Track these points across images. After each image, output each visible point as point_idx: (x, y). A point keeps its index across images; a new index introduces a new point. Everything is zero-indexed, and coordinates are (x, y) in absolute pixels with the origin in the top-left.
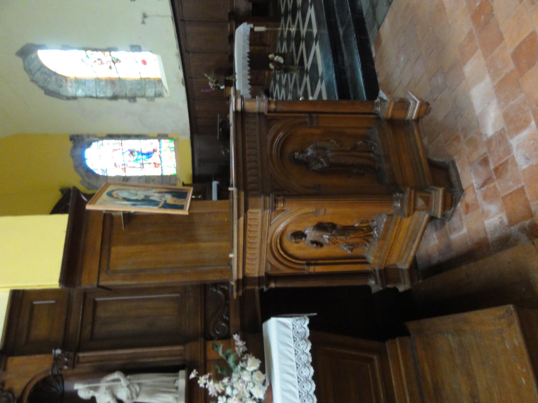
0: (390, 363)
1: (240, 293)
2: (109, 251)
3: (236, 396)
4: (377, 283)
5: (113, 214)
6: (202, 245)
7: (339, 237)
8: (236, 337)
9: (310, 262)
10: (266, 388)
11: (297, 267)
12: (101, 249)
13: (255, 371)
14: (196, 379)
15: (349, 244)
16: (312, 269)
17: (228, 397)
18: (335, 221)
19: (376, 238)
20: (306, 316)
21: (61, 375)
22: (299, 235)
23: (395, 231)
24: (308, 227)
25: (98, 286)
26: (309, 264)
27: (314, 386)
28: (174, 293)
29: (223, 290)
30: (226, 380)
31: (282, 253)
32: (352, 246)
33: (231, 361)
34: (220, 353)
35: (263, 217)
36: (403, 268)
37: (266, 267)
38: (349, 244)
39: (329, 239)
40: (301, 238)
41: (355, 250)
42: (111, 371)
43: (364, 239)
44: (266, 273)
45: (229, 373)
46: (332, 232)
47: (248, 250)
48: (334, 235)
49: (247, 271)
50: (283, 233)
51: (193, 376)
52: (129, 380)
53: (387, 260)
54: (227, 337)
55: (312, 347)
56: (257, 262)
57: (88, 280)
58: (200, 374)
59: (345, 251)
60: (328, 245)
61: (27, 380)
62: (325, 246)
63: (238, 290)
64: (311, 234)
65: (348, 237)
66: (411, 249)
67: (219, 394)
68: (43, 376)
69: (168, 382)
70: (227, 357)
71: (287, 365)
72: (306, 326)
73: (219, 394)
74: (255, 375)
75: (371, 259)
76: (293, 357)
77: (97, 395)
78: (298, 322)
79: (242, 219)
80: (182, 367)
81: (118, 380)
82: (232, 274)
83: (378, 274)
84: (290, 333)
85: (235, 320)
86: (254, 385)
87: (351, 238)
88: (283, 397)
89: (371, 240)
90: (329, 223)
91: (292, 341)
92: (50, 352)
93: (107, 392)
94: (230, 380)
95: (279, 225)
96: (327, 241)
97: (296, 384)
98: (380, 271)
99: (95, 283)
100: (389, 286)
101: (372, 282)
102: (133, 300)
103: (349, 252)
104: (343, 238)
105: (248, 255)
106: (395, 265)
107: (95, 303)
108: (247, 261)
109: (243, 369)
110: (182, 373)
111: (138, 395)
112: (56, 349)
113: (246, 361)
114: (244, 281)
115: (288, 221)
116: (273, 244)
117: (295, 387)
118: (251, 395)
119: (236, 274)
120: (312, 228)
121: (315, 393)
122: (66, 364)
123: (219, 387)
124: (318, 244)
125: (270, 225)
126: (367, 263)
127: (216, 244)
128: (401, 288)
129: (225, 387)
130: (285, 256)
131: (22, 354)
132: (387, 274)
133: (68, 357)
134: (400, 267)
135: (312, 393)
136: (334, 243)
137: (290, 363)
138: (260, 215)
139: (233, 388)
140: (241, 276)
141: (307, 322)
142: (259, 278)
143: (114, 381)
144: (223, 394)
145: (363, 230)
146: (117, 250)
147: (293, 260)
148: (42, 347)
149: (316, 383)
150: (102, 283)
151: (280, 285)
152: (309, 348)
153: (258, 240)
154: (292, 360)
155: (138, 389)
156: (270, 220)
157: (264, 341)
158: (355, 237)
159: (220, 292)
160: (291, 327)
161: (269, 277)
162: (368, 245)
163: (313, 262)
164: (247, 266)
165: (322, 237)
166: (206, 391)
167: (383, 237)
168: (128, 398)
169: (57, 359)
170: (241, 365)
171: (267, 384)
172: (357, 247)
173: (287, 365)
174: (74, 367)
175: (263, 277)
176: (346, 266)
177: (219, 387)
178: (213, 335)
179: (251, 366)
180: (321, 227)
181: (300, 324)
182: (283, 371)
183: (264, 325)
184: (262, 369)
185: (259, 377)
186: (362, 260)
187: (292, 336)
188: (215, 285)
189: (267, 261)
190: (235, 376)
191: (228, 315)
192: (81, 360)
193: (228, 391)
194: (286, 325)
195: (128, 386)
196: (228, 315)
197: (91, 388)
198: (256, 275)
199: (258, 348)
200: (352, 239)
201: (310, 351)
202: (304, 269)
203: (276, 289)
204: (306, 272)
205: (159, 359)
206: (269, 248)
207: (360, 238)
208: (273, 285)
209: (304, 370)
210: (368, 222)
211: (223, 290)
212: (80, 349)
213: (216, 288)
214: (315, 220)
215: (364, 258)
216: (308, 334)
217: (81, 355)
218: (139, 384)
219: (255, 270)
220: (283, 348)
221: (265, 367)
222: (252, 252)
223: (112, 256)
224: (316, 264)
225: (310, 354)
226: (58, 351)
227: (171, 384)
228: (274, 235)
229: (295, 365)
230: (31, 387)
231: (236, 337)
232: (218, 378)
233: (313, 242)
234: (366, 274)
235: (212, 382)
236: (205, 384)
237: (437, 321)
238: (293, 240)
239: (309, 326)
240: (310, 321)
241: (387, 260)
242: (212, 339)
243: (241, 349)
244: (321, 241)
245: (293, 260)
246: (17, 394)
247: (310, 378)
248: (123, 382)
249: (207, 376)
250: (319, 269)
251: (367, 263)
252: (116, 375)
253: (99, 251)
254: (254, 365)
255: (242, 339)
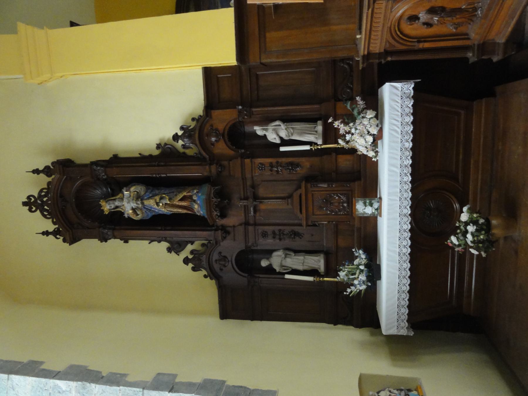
0: (474, 117)
1: (365, 65)
2: (265, 36)
3: (358, 133)
4: (473, 55)
5: (264, 5)
6: (334, 28)
7: (446, 19)
8: (358, 98)
9: (420, 39)
10: (378, 128)
11: (409, 44)
12: (259, 34)
13: (372, 118)
14: (332, 123)
15: (455, 24)
16: (421, 46)
17: (353, 134)
18: (445, 5)
19: (479, 17)
20: (412, 81)
21: (243, 122)
22: (414, 18)
23: (497, 10)
24: (422, 11)
25: (261, 63)
26: (419, 42)
27: (412, 127)
28: (312, 68)
29: (348, 64)
30: (351, 124)
31: (398, 33)
32: (457, 25)
33: (355, 112)
34: (348, 107)
35: (386, 7)
36: (500, 42)
37: (386, 44)
38: (455, 24)
39: (438, 20)
40: (415, 21)
41: (459, 28)
42: (275, 120)
43: (469, 19)
44: (384, 50)
45: (354, 120)
46: (441, 14)
47: (373, 33)
48: (442, 17)
49: (371, 48)
50: (401, 17)
51: (330, 121)
52: (286, 125)
53: (486, 36)
54: (352, 99)
55: (414, 103)
56: (378, 42)
57: (254, 59)
58: (335, 120)
59: (452, 29)
60: (437, 25)
61: (225, 124)
62: (434, 26)
63: (363, 63)
64: (423, 17)
65: (454, 18)
66: (509, 26)
67: (347, 133)
68: (233, 122)
69: (311, 128)
70: (353, 109)
71: (394, 114)
72: (411, 88)
73: (347, 133)
74: (372, 120)
75: (473, 35)
76: (400, 110)
77: (267, 134)
78: (406, 86)
79: (370, 10)
80: (320, 119)
81: (280, 125)
82: (357, 52)
83: (476, 48)
84: (399, 93)
85: (357, 87)
86: (371, 126)
87: (457, 19)
88: (390, 133)
89: (475, 19)
90: (439, 7)
91: (400, 98)
92: (235, 108)
93: (273, 132)
94: (354, 124)
95: (398, 11)
96: (436, 22)
97: (400, 126)
98: (479, 45)
99: (259, 61)
100: (483, 57)
101: (470, 55)
102: (296, 72)
103: (454, 30)
104: (449, 19)
105: (372, 37)
106: (493, 40)
107: (257, 75)
108: (372, 41)
109: (363, 117)
110: (319, 122)
111: (292, 135)
112: (238, 106)
113: (366, 113)
114: (368, 57)
115: (405, 8)
116: (392, 26)
117: (398, 128)
118: (369, 132)
119: (362, 50)
120: (424, 12)
121: (412, 132)
122: (246, 115)
123: (347, 129)
124: (428, 25)
125: (391, 12)
126: (469, 39)
127: (344, 27)
128: (495, 59)
129: (351, 128)
130: (401, 36)
131: (218, 109)
132: (484, 47)
133: (246, 111)
134: (498, 41)
135: (410, 132)
136: (441, 24)
137: (397, 113)
138: (384, 4)
139: (356, 129)
140: (366, 53)
141: (413, 86)
142: (380, 54)
143: (276, 126)
144: (349, 133)
145: (467, 11)
146: (271, 35)
147: (407, 39)
148: (230, 105)
149: (413, 126)
150: (264, 61)
151: (394, 58)
152: (412, 103)
153: (381, 24)
154: (398, 111)
155: (292, 131)
156: (392, 8)
157: (379, 102)
158: (461, 18)
159: (346, 66)
160: (400, 89)
161: (387, 53)
162: (472, 23)
163: (422, 40)
164: (371, 45)
165: (432, 18)
166: (338, 130)
167: (485, 16)
168: (286, 136)
169: (240, 112)
170: (362, 115)
171: (380, 126)
172: (462, 26)
173: (394, 114)
174: (250, 117)
175: (382, 53)
176: (445, 42)
177: (347, 129)
178: (340, 98)
179: (369, 115)
180: (432, 11)
181: (408, 87)
182: (391, 118)
183: (379, 90)
184: (376, 117)
185: (374, 122)
186: (465, 36)
187: (400, 96)
188: (343, 60)
189: (387, 41)
190: (358, 122)
191: (352, 84)
192: (255, 113)
193: (353, 131)
194: (396, 88)
195: (286, 129)
196: (352, 84)
197: (264, 129)
198: (377, 52)
199: (374, 103)
200: (457, 19)
201: (412, 106)
202: (415, 46)
203: (392, 61)
204: (416, 48)
205: (304, 113)
206: (388, 30)
207: (464, 18)
208: (389, 59)
209: (406, 118)
210: (474, 3)
211: (348, 64)
212: (251, 107)
213: (343, 63)
214: (428, 6)
215: (467, 34)
216: (412, 94)
217: (254, 110)
218: (293, 128)
219: (377, 47)
220: (393, 103)
221: (379, 116)
222: (375, 34)
223: (267, 40)
224: (425, 41)
225: (412, 108)
226: (240, 107)
227: (313, 129)
228: (393, 23)
229: (400, 114)
230: (227, 128)
231: (358, 98)
232: (346, 124)
233: (424, 24)
234: (467, 48)
235: (342, 125)
236: (338, 126)
237: (516, 83)
238: (409, 23)
239: (413, 88)
240: (415, 85)
241: (486, 36)
242: (340, 100)
243: (362, 106)
244: (431, 22)
245: (407, 39)
246: (221, 132)
247: (410, 123)
248: (283, 126)
249: (340, 122)
250: (427, 45)
251: (469, 39)
252: (277, 123)
253: (258, 36)
254: (371, 114)
255: (362, 99)
